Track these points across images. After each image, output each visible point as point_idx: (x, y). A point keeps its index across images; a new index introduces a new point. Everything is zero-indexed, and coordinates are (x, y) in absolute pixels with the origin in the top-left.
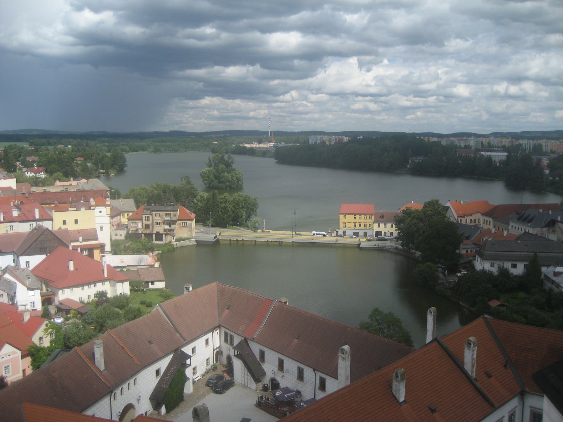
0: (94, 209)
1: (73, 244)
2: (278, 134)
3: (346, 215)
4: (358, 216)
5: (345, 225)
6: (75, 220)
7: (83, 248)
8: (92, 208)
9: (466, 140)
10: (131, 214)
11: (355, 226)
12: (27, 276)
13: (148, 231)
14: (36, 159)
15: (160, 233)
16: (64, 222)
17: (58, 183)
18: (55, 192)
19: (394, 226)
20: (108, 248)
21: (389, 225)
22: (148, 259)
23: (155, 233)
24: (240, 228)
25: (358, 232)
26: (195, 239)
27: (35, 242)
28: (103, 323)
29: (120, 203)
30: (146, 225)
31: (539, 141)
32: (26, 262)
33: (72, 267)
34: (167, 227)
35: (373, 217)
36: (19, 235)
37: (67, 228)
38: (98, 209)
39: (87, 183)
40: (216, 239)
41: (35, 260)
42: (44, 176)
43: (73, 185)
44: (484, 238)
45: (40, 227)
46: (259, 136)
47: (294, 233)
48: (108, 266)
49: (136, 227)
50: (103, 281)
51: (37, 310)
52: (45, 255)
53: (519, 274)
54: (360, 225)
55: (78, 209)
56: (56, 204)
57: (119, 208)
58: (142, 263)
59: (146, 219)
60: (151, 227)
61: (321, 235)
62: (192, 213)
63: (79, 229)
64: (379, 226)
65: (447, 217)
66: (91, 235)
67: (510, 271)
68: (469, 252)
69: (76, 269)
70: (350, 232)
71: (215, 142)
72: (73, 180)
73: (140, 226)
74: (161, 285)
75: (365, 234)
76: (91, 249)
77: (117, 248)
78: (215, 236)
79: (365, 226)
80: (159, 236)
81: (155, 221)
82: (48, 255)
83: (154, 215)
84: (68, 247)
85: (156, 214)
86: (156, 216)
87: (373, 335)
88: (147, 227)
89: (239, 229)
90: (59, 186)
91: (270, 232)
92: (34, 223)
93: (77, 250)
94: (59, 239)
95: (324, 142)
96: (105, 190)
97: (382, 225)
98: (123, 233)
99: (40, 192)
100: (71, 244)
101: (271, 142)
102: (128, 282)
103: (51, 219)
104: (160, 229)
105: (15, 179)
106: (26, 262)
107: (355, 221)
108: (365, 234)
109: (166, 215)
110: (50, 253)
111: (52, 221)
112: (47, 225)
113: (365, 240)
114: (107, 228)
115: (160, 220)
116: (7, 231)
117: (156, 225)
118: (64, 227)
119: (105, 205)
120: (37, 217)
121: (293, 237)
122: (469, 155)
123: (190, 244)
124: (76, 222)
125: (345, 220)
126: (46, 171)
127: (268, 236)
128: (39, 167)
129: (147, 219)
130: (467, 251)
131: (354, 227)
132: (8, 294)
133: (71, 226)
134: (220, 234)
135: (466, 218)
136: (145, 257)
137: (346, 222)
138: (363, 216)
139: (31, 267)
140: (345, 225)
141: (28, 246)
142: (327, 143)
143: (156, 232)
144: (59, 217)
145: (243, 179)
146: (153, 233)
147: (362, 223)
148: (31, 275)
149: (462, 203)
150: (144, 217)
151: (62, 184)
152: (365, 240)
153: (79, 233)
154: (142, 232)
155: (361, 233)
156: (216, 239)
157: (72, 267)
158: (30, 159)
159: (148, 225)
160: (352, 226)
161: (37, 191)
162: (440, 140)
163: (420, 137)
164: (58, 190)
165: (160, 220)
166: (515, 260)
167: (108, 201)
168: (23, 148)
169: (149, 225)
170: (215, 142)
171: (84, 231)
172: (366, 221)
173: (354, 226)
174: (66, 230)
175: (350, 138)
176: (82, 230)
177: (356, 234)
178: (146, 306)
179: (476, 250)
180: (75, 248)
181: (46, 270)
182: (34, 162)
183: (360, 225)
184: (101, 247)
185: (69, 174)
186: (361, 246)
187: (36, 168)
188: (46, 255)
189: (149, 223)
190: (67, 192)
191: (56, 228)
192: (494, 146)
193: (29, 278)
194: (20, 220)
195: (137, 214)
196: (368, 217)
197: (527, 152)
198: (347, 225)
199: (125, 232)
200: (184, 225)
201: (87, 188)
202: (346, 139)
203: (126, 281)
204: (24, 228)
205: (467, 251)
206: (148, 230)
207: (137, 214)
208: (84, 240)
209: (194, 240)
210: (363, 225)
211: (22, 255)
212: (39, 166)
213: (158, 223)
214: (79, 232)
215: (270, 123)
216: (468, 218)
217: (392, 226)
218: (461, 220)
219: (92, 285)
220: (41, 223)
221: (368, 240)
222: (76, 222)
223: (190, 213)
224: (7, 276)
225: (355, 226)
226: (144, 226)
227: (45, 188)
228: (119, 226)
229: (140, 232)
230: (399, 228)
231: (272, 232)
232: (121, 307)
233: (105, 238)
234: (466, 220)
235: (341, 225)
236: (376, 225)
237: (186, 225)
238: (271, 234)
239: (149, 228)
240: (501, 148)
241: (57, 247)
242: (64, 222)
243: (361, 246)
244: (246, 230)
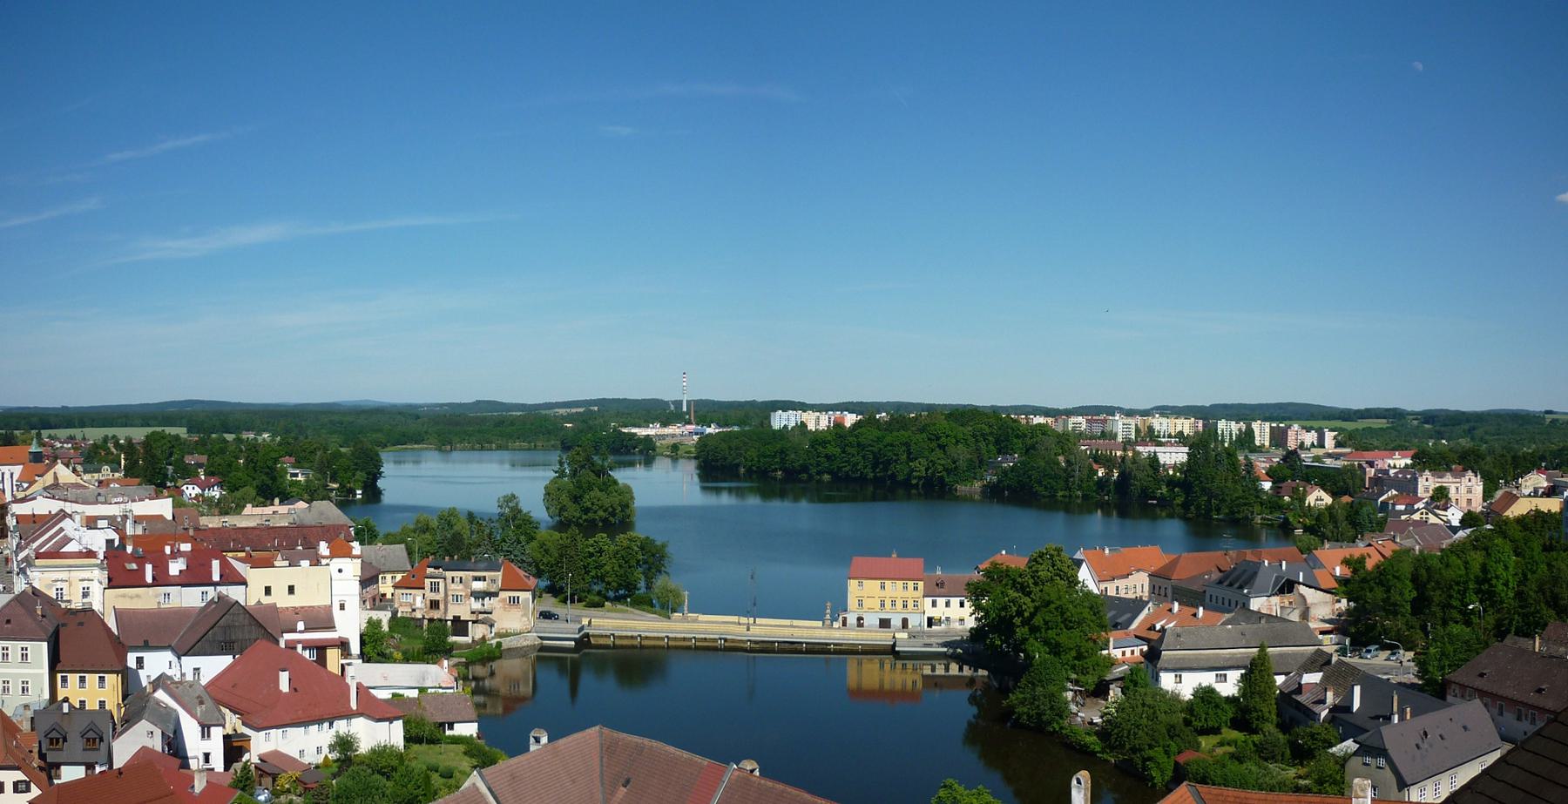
0: (328, 565)
1: (288, 636)
2: (705, 411)
3: (864, 581)
5: (861, 604)
6: (289, 587)
7: (308, 646)
8: (324, 562)
9: (1105, 421)
10: (399, 577)
11: (883, 605)
12: (198, 697)
13: (436, 615)
14: (204, 459)
15: (462, 619)
16: (268, 591)
17: (249, 509)
18: (246, 528)
19: (967, 604)
20: (355, 648)
21: (955, 601)
22: (438, 675)
23: (452, 618)
24: (632, 609)
25: (890, 619)
26: (536, 632)
27: (213, 627)
29: (379, 551)
30: (431, 601)
32: (194, 669)
33: (284, 686)
34: (477, 605)
35: (921, 584)
36: (182, 614)
37: (275, 604)
38: (337, 563)
39: (308, 510)
40: (583, 632)
41: (213, 666)
42: (218, 494)
43: (279, 513)
44: (1157, 623)
45: (221, 598)
46: (664, 413)
47: (751, 620)
48: (359, 687)
49: (411, 605)
50: (349, 715)
52: (232, 656)
54: (894, 603)
55: (293, 564)
56: (247, 553)
57: (374, 564)
58: (426, 681)
59: (431, 589)
60: (442, 606)
62: (531, 577)
63: (297, 605)
64: (934, 604)
65: (1080, 582)
66: (322, 619)
68: (1128, 654)
69: (294, 689)
70: (872, 620)
71: (568, 425)
72: (281, 502)
73: (419, 603)
74: (468, 729)
75: (905, 623)
76: (321, 649)
77: (374, 647)
78: (579, 626)
79: (905, 606)
80: (460, 626)
81: (450, 593)
82: (237, 656)
83: (449, 580)
84: (277, 642)
85: (453, 578)
86: (453, 582)
88: (434, 605)
89: (632, 612)
90: (252, 516)
91: (700, 619)
92: (210, 589)
93: (295, 648)
94: (261, 625)
95: (803, 425)
96: (346, 525)
98: (384, 617)
99: (216, 526)
100: (282, 636)
101: (689, 423)
102: (401, 721)
103: (244, 583)
104: (463, 611)
105: (171, 499)
106: (194, 669)
107: (883, 593)
108: (905, 623)
109: (476, 579)
110: (241, 653)
111: (244, 587)
112: (235, 593)
113: (905, 635)
114: (353, 603)
115: (461, 590)
116: (159, 603)
117: (453, 600)
118: (266, 600)
119: (348, 554)
120: (216, 577)
121: (748, 630)
122: (1111, 454)
123: (525, 644)
124: (291, 590)
126: (221, 485)
127: (695, 626)
128: (209, 475)
129: (435, 589)
130: (1124, 653)
132: (162, 732)
133: (281, 600)
134: (590, 622)
135: (1117, 582)
136: (432, 668)
139: (204, 681)
140: (861, 604)
141: (199, 638)
142: (811, 427)
143: (454, 617)
144: (257, 578)
146: (447, 618)
148: (206, 698)
150: (428, 581)
151: (259, 510)
152: (905, 635)
153: (297, 614)
154: (423, 616)
155: (896, 622)
156: (583, 632)
157: (284, 686)
158: (190, 460)
159: (435, 601)
161: (210, 526)
162: (1049, 421)
163: (1008, 416)
164: (252, 524)
165: (461, 590)
166: (1220, 668)
167: (356, 548)
168: (177, 437)
169: (438, 601)
170: (568, 425)
171: (306, 611)
174: (273, 607)
175: (859, 417)
176: (302, 608)
177: (884, 623)
178: (440, 776)
179: (1141, 650)
180: (291, 646)
181: (233, 687)
182: (200, 465)
183: (894, 603)
184: (343, 645)
185: (270, 491)
186: (897, 649)
187: (203, 477)
188: (234, 658)
189: (439, 597)
190: (269, 528)
191: (252, 602)
192: (1162, 433)
193: (201, 703)
194: (186, 580)
195: (413, 577)
197: (1226, 445)
199: (389, 614)
200: (514, 602)
201: (310, 519)
202: (850, 419)
203: (397, 718)
204: (192, 598)
205: (1124, 653)
206: (437, 611)
207: (413, 577)
208: (307, 630)
209: (535, 634)
210: (899, 604)
211: (184, 655)
212: (209, 474)
213: (457, 596)
214: (298, 612)
215: (685, 384)
216: (1121, 583)
217: (962, 605)
218: (1106, 588)
219: (326, 725)
220: (223, 589)
221: (912, 636)
222: (291, 590)
223: (526, 576)
224: (161, 695)
225: (883, 605)
226: (428, 603)
227: (226, 520)
228: (379, 602)
229: (419, 615)
230: (978, 607)
231: (702, 617)
232: (386, 773)
233: (350, 625)
234: (1117, 588)
235: (852, 602)
236: (929, 601)
237: (518, 602)
238: (702, 622)
239: (438, 608)
240: (1175, 437)
241: (255, 640)
242: (268, 591)
243: (897, 649)
244: (644, 613)
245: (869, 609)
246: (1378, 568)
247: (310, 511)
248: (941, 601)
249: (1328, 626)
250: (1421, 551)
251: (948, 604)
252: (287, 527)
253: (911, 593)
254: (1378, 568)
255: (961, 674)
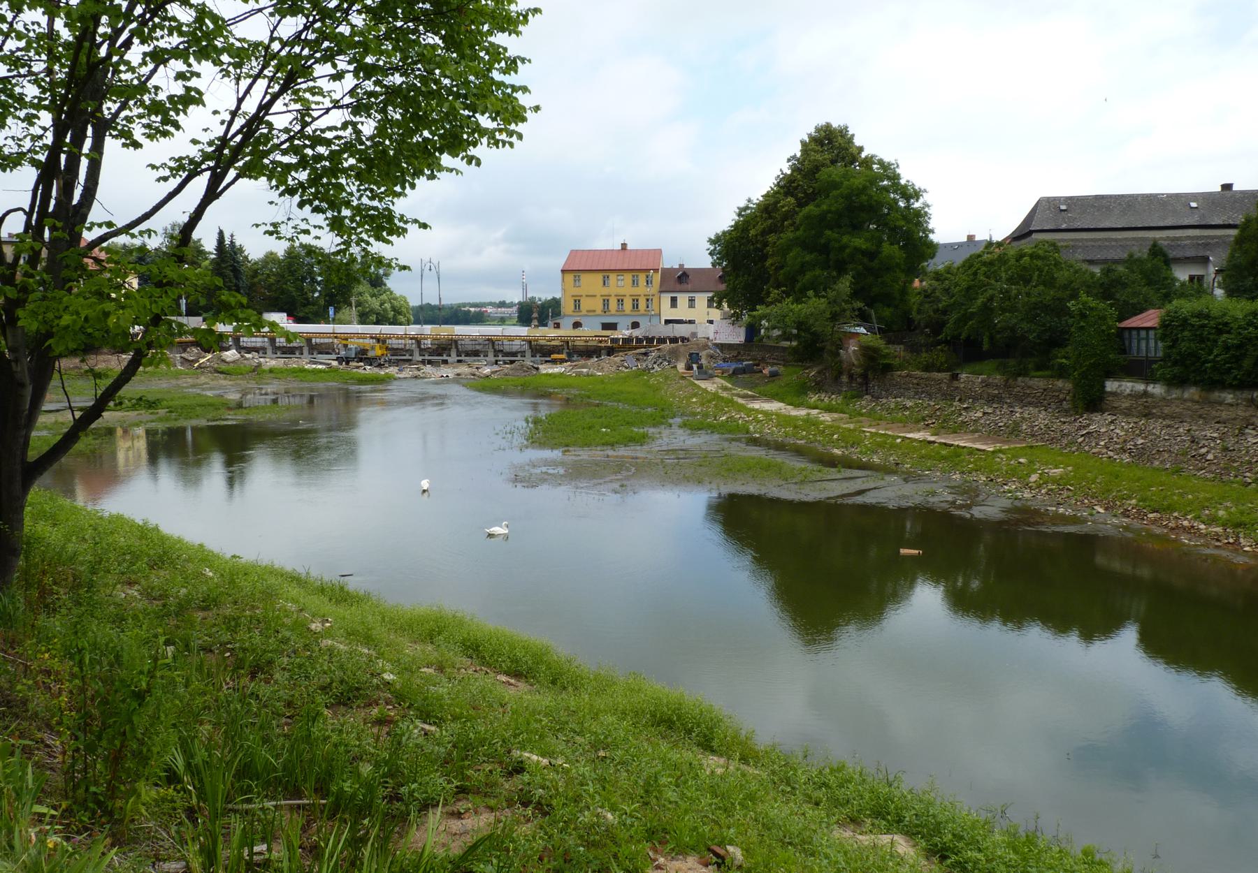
11: (606, 303)
28: (903, 267)
31: (556, 471)
51: (1235, 188)
54: (620, 302)
64: (674, 302)
79: (635, 306)
87: (925, 375)
107: (605, 291)
125: (576, 291)
138: (628, 277)
149: (425, 484)
160: (598, 306)
172: (636, 291)
198: (586, 305)
225: (606, 303)
236: (666, 299)
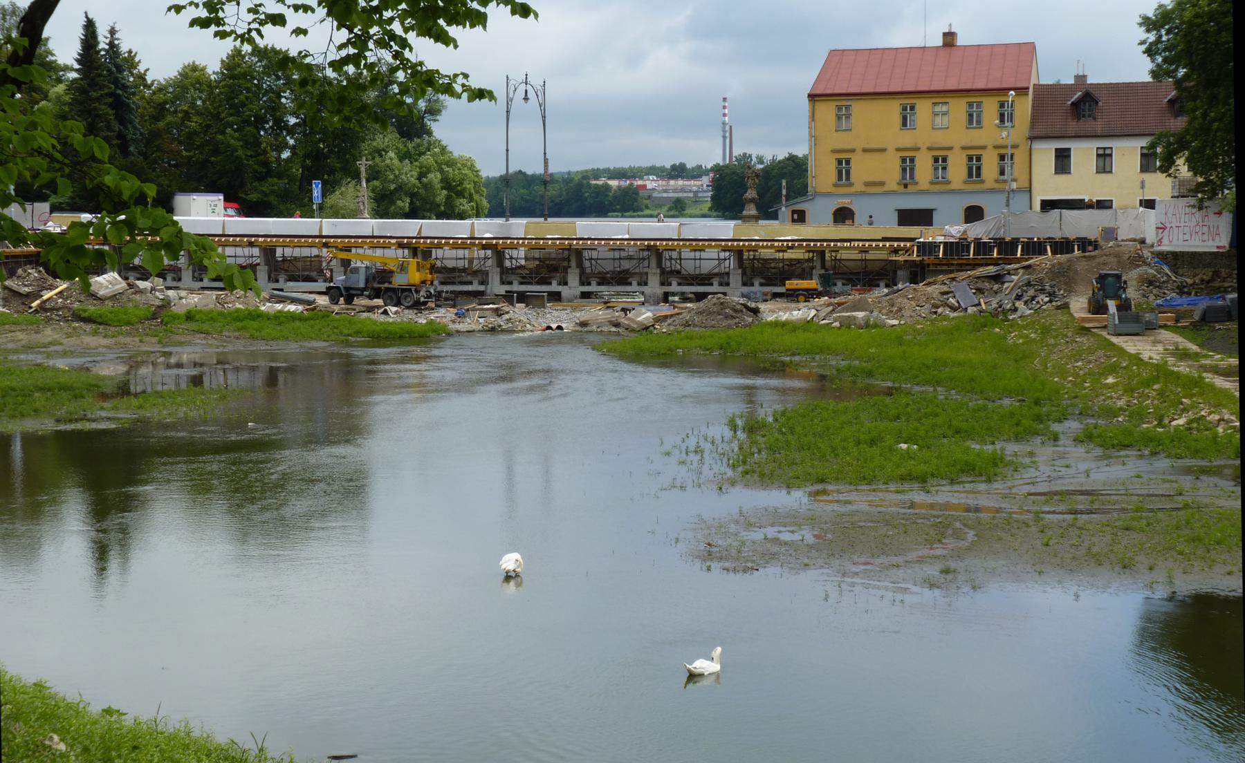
4: (923, 108)
11: (908, 165)
53: (1048, 588)
54: (940, 162)
61: (340, 527)
64: (1063, 161)
67: (720, 431)
79: (974, 171)
97: (1083, 153)
107: (907, 139)
125: (842, 141)
131: (840, 178)
137: (917, 149)
145: (216, 34)
147: (990, 147)
173: (840, 173)
183: (940, 162)
196: (990, 108)
198: (862, 170)
210: (957, 170)
225: (908, 165)
236: (1045, 154)
245: (867, 184)
246: (1040, 573)
247: (719, 683)
248: (1083, 153)
249: (103, 45)
250: (1226, 153)
251: (1104, 158)
252: (1216, 322)
253: (990, 133)
254: (1040, 573)
255: (1037, 206)
